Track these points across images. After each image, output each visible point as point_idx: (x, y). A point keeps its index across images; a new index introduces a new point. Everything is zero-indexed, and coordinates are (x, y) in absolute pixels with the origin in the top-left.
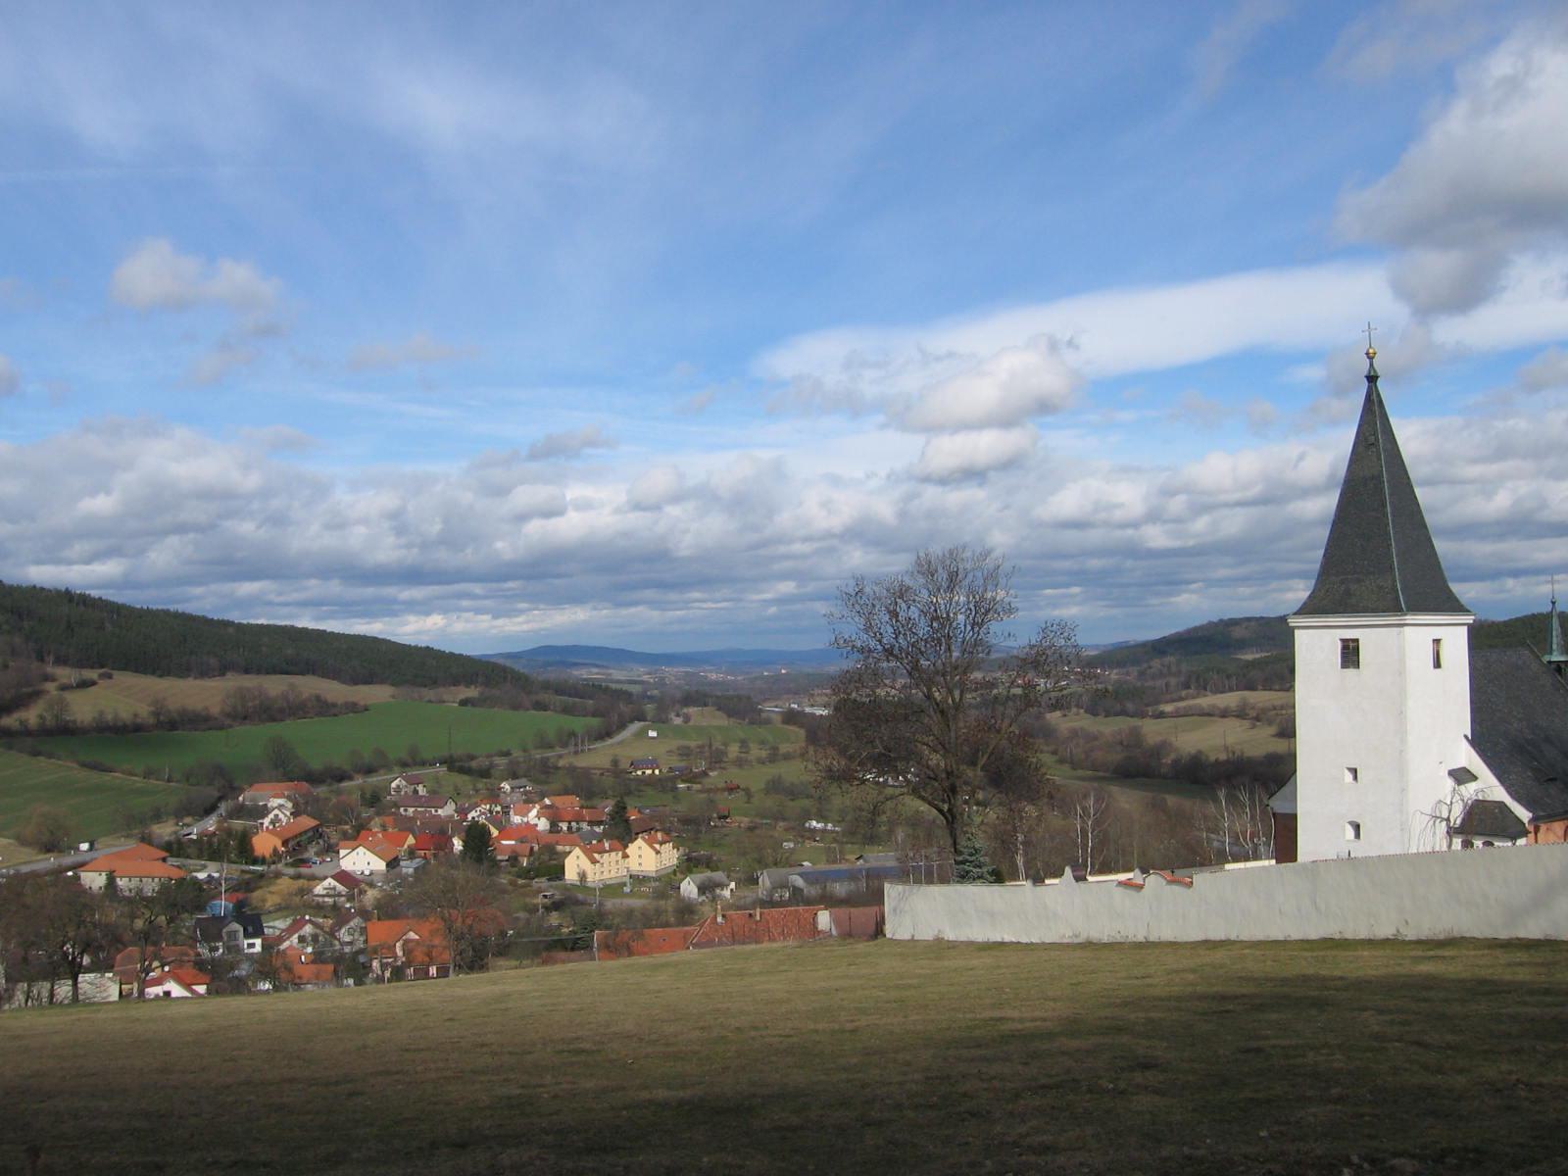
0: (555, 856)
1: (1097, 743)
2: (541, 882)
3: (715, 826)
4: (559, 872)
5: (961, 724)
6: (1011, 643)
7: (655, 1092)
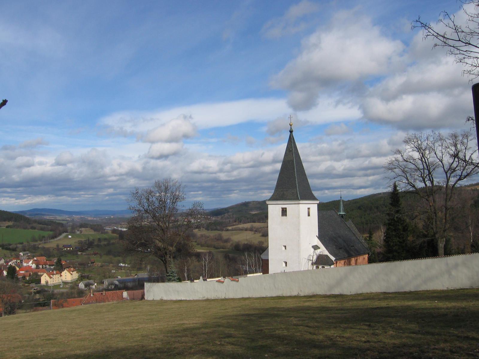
0: (38, 276)
1: (208, 239)
2: (33, 285)
3: (90, 266)
4: (40, 281)
5: (169, 233)
6: (183, 208)
7: (76, 352)
